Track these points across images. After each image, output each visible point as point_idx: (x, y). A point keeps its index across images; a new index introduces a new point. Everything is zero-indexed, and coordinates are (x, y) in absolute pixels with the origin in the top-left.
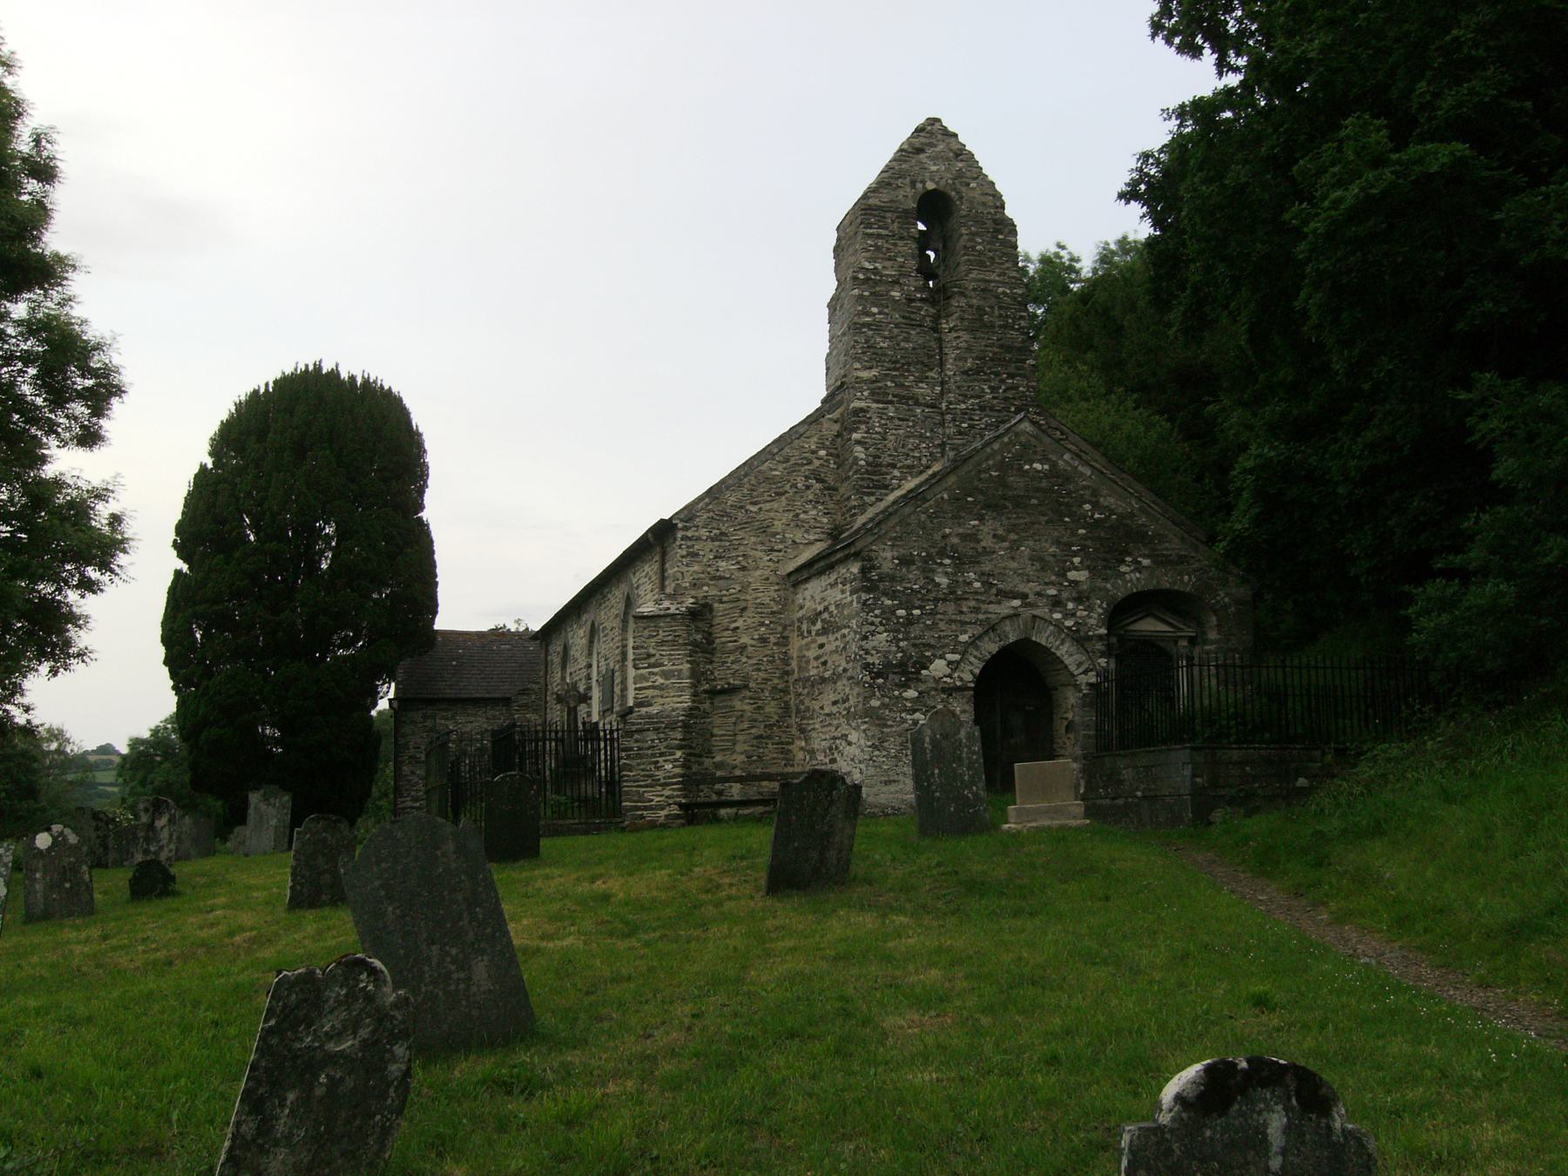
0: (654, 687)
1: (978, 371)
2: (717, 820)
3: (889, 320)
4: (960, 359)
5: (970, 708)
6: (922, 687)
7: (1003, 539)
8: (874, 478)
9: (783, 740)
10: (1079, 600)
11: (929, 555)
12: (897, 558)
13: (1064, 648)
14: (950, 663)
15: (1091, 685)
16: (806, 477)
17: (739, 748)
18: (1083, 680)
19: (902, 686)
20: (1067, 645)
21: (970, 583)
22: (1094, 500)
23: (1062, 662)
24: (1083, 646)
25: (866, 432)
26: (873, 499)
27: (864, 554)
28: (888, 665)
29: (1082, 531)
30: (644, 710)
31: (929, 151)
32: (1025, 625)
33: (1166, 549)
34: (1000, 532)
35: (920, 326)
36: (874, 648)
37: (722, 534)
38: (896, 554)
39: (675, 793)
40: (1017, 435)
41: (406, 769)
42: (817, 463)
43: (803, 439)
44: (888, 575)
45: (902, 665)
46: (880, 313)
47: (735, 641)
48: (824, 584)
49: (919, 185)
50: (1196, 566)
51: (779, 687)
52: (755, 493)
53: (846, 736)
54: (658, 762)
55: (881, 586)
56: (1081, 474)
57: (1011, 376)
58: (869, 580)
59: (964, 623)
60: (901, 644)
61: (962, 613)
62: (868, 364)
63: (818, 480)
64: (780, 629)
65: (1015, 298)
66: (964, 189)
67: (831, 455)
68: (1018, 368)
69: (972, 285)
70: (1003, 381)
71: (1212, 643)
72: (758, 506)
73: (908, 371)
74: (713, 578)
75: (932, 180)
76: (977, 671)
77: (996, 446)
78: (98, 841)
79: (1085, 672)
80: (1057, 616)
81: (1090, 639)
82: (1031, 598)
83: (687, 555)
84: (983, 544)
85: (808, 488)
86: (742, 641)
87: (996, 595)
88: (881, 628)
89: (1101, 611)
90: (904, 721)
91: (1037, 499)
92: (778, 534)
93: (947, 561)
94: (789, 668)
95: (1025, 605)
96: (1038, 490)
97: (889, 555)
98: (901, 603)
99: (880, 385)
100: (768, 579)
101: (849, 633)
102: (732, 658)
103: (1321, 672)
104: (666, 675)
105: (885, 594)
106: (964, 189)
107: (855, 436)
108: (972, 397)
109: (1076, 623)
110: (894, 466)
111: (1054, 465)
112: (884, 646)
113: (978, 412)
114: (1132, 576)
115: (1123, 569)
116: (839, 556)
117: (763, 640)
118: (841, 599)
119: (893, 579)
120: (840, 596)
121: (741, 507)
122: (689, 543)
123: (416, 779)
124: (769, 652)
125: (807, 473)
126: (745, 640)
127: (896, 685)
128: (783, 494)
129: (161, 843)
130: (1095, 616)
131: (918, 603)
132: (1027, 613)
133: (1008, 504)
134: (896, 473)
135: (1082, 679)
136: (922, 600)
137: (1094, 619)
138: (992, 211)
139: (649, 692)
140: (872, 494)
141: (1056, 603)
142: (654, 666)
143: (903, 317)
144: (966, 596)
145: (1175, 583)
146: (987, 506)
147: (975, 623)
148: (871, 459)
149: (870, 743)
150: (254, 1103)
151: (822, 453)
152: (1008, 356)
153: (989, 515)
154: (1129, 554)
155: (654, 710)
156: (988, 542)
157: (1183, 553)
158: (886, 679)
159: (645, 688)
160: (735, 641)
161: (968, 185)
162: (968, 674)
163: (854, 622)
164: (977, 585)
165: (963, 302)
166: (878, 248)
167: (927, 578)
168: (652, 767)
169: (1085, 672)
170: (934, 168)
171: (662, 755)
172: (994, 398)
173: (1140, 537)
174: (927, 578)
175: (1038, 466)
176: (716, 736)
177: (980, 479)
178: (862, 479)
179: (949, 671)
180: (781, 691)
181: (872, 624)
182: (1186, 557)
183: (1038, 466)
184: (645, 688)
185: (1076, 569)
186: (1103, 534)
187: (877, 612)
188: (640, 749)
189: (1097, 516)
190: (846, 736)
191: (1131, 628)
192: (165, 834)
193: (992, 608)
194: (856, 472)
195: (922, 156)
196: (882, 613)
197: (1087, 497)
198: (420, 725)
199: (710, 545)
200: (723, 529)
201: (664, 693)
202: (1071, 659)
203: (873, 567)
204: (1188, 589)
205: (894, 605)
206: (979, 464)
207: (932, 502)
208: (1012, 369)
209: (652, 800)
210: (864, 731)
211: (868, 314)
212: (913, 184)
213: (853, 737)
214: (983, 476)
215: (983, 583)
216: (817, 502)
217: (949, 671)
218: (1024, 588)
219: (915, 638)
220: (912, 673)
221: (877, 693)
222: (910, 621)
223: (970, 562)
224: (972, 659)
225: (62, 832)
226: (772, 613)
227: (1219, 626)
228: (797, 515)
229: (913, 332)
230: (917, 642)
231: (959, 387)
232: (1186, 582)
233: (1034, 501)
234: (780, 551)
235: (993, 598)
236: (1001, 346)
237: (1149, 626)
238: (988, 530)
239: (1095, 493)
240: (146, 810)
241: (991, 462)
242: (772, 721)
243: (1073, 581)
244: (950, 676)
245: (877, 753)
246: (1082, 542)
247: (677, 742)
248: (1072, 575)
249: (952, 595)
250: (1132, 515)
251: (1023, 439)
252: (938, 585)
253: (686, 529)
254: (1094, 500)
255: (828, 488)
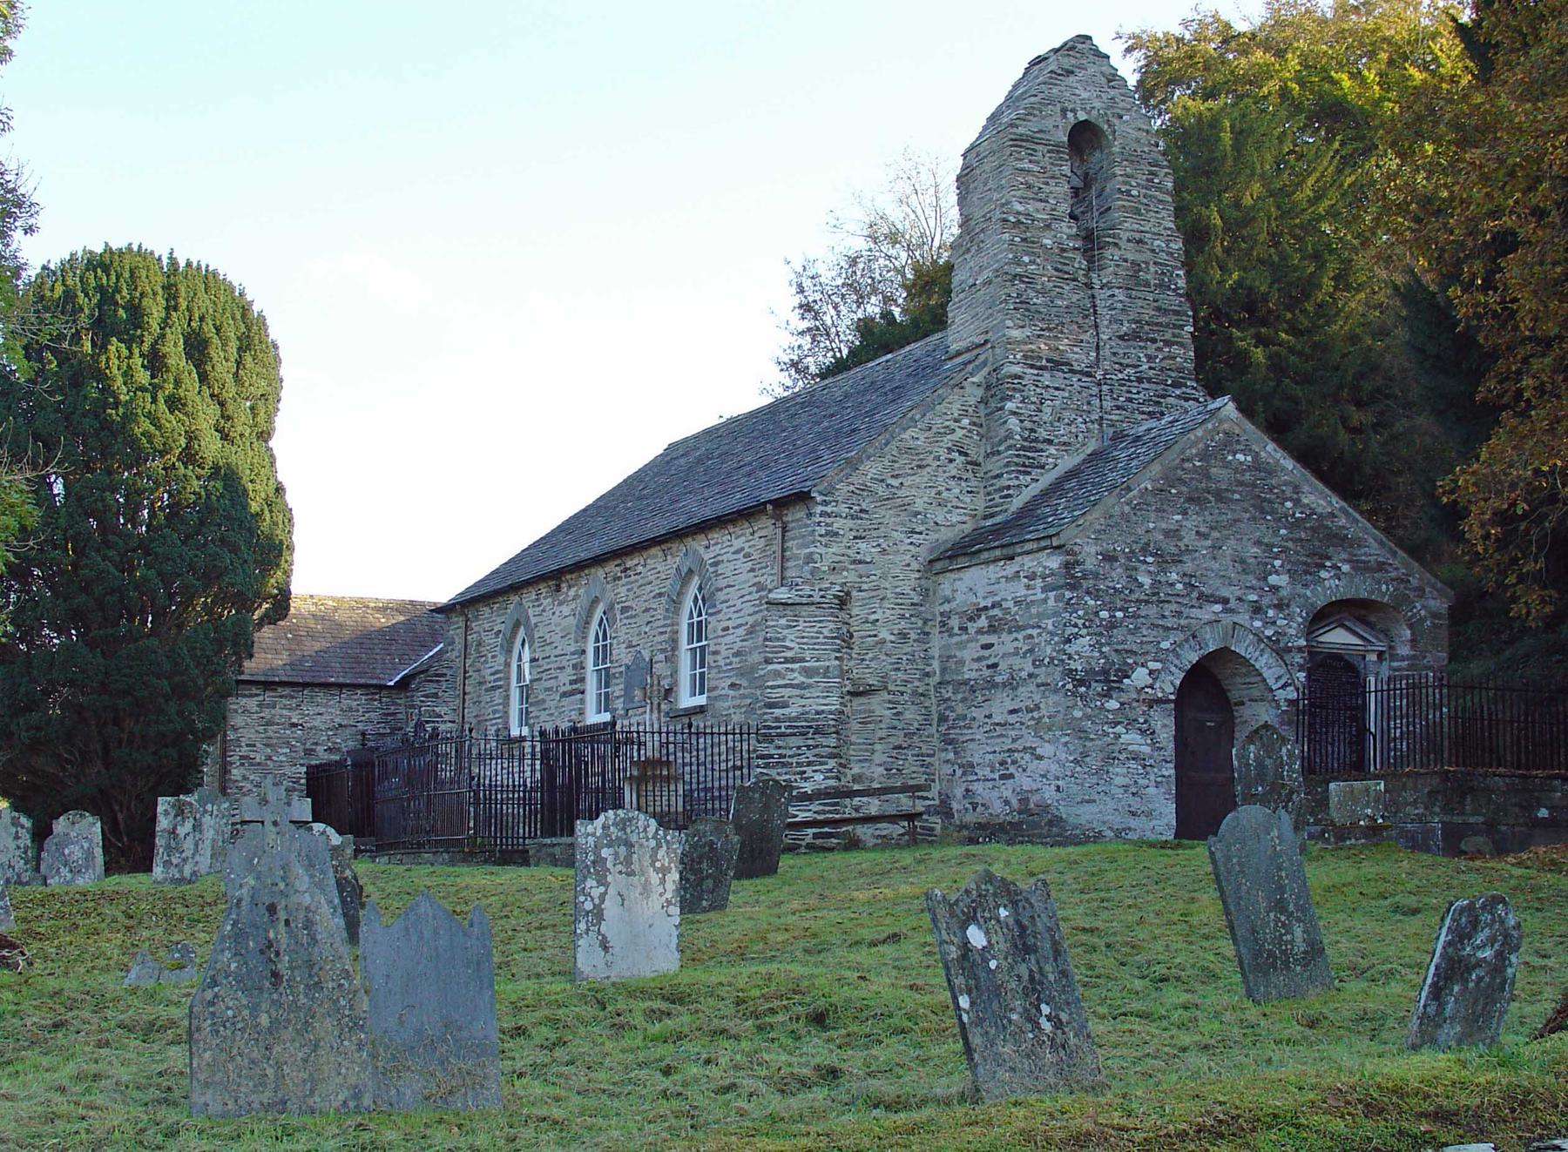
0: (792, 686)
1: (1135, 336)
2: (853, 844)
3: (1041, 272)
4: (1116, 321)
5: (1171, 722)
6: (1124, 698)
7: (1204, 536)
8: (1029, 454)
9: (924, 751)
10: (1279, 607)
11: (1132, 552)
12: (1101, 554)
13: (1263, 661)
14: (1151, 672)
15: (1290, 702)
16: (949, 449)
17: (879, 758)
18: (1281, 695)
19: (1105, 696)
20: (1266, 656)
21: (1172, 585)
22: (1295, 496)
23: (1261, 675)
24: (1282, 658)
25: (1021, 402)
26: (1028, 478)
27: (1068, 547)
28: (1090, 672)
29: (1283, 532)
30: (778, 712)
31: (1081, 74)
32: (1226, 634)
33: (1365, 554)
34: (1202, 530)
35: (1074, 280)
36: (1077, 653)
37: (861, 511)
38: (1099, 549)
39: (827, 808)
40: (1221, 422)
41: (236, 773)
42: (960, 433)
43: (944, 404)
44: (1092, 573)
45: (1105, 672)
46: (1033, 262)
47: (875, 636)
48: (993, 577)
49: (1070, 115)
50: (1393, 574)
51: (920, 690)
52: (896, 465)
53: (1035, 749)
54: (805, 772)
55: (1085, 584)
56: (1283, 469)
57: (1168, 343)
58: (1073, 577)
59: (1168, 629)
60: (1104, 649)
61: (1164, 616)
62: (1022, 324)
63: (961, 453)
64: (920, 623)
65: (1172, 254)
66: (1116, 121)
67: (974, 424)
68: (1174, 335)
69: (1125, 236)
70: (1159, 349)
71: (1403, 659)
72: (900, 480)
73: (1062, 332)
74: (854, 562)
75: (1084, 109)
76: (1178, 683)
77: (1199, 433)
78: (18, 853)
79: (1284, 687)
80: (1258, 624)
81: (1289, 650)
82: (1233, 604)
83: (827, 534)
84: (1186, 541)
85: (951, 461)
86: (881, 636)
87: (1198, 599)
88: (1084, 632)
89: (1300, 620)
90: (1107, 734)
91: (1240, 493)
92: (920, 513)
93: (1150, 559)
94: (928, 669)
95: (1225, 611)
96: (1241, 483)
97: (1093, 550)
98: (1104, 604)
99: (1033, 347)
100: (909, 565)
101: (1040, 635)
102: (870, 655)
103: (1430, 690)
104: (808, 672)
105: (1088, 593)
106: (1116, 121)
107: (1009, 405)
108: (1128, 366)
109: (1276, 633)
110: (1050, 442)
111: (1256, 455)
112: (1087, 652)
113: (1135, 384)
114: (1331, 585)
115: (1323, 574)
116: (1028, 546)
117: (903, 635)
118: (1026, 596)
119: (1096, 576)
120: (1024, 592)
121: (882, 481)
122: (828, 520)
123: (248, 786)
124: (909, 649)
125: (950, 445)
126: (884, 634)
127: (1099, 694)
128: (925, 467)
129: (184, 855)
130: (1295, 625)
131: (1119, 604)
132: (1228, 619)
133: (1210, 497)
134: (1052, 450)
135: (1281, 695)
136: (1126, 601)
137: (1292, 628)
138: (1146, 149)
139: (787, 692)
140: (1029, 473)
141: (1257, 610)
142: (793, 660)
143: (1057, 269)
144: (1169, 598)
145: (1373, 593)
146: (1190, 500)
147: (1177, 629)
148: (1027, 434)
149: (1071, 758)
150: (1437, 993)
151: (965, 422)
152: (1163, 320)
153: (1193, 508)
154: (1329, 558)
155: (793, 711)
156: (1189, 538)
157: (1381, 559)
158: (1089, 687)
159: (779, 686)
160: (875, 636)
161: (1121, 117)
162: (1168, 685)
163: (1050, 622)
164: (1179, 586)
165: (1117, 254)
166: (1029, 187)
167: (1130, 577)
168: (798, 777)
169: (1284, 687)
170: (1085, 95)
171: (809, 763)
172: (1150, 368)
173: (1339, 539)
174: (1130, 577)
175: (1240, 457)
176: (855, 744)
177: (1183, 469)
178: (1018, 456)
179: (1151, 681)
180: (922, 695)
181: (1076, 626)
182: (1384, 563)
183: (1240, 457)
184: (779, 686)
185: (1277, 573)
186: (1303, 535)
187: (1081, 613)
188: (781, 756)
189: (1298, 515)
190: (1035, 749)
191: (1321, 639)
192: (188, 845)
193: (1195, 612)
194: (1009, 448)
195: (1071, 78)
196: (1085, 614)
197: (1288, 494)
198: (255, 716)
199: (850, 523)
200: (864, 506)
201: (806, 693)
202: (1270, 671)
203: (1078, 563)
204: (1386, 600)
205: (1097, 606)
206: (1183, 452)
207: (1135, 492)
208: (1168, 336)
209: (796, 816)
210: (1066, 744)
211: (1019, 263)
212: (1064, 111)
213: (1046, 750)
214: (1186, 465)
215: (1185, 584)
216: (960, 479)
217: (1151, 681)
218: (1225, 592)
219: (1118, 643)
220: (1114, 681)
221: (1079, 703)
222: (1112, 625)
223: (1173, 561)
224: (1173, 669)
225: (324, 832)
226: (912, 604)
227: (1413, 640)
228: (939, 493)
229: (1067, 288)
230: (1120, 647)
231: (1114, 354)
232: (1384, 592)
233: (1237, 496)
234: (921, 533)
235: (1194, 602)
236: (1158, 309)
237: (1337, 637)
238: (1192, 523)
239: (1297, 489)
240: (166, 813)
241: (1194, 451)
242: (912, 729)
243: (1274, 587)
244: (1151, 687)
245: (1078, 769)
246: (1284, 544)
247: (830, 750)
248: (1273, 579)
249: (1155, 596)
250: (1333, 515)
251: (1226, 426)
252: (1141, 585)
253: (825, 503)
254: (1295, 496)
255: (971, 463)
